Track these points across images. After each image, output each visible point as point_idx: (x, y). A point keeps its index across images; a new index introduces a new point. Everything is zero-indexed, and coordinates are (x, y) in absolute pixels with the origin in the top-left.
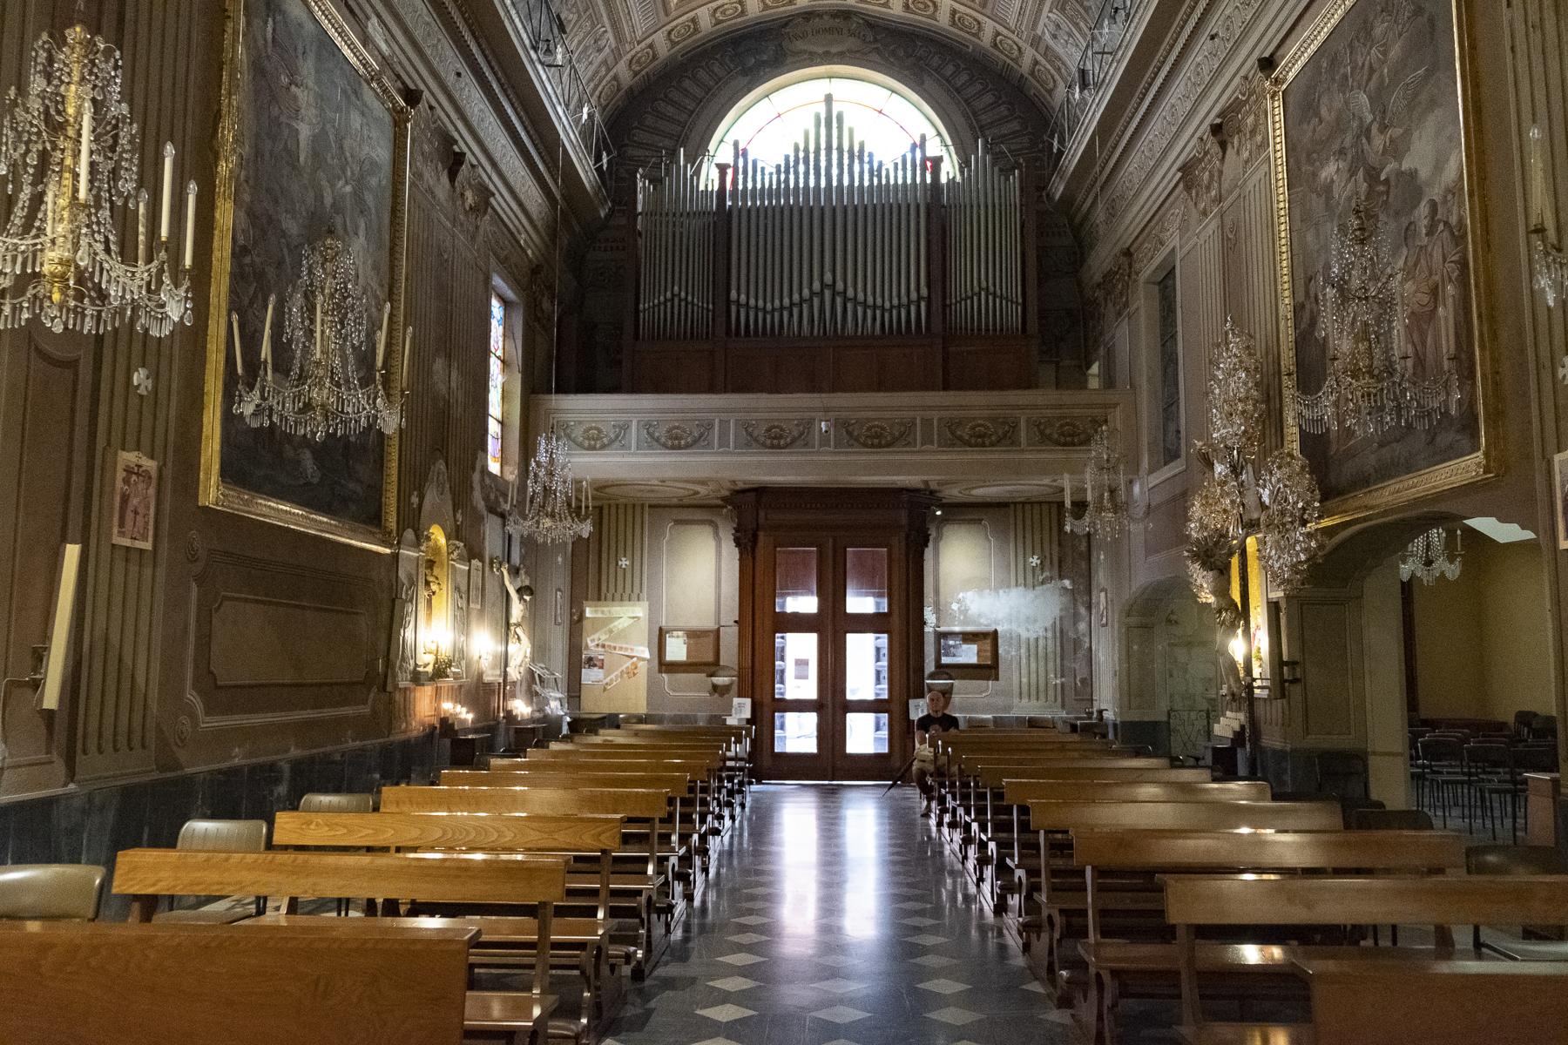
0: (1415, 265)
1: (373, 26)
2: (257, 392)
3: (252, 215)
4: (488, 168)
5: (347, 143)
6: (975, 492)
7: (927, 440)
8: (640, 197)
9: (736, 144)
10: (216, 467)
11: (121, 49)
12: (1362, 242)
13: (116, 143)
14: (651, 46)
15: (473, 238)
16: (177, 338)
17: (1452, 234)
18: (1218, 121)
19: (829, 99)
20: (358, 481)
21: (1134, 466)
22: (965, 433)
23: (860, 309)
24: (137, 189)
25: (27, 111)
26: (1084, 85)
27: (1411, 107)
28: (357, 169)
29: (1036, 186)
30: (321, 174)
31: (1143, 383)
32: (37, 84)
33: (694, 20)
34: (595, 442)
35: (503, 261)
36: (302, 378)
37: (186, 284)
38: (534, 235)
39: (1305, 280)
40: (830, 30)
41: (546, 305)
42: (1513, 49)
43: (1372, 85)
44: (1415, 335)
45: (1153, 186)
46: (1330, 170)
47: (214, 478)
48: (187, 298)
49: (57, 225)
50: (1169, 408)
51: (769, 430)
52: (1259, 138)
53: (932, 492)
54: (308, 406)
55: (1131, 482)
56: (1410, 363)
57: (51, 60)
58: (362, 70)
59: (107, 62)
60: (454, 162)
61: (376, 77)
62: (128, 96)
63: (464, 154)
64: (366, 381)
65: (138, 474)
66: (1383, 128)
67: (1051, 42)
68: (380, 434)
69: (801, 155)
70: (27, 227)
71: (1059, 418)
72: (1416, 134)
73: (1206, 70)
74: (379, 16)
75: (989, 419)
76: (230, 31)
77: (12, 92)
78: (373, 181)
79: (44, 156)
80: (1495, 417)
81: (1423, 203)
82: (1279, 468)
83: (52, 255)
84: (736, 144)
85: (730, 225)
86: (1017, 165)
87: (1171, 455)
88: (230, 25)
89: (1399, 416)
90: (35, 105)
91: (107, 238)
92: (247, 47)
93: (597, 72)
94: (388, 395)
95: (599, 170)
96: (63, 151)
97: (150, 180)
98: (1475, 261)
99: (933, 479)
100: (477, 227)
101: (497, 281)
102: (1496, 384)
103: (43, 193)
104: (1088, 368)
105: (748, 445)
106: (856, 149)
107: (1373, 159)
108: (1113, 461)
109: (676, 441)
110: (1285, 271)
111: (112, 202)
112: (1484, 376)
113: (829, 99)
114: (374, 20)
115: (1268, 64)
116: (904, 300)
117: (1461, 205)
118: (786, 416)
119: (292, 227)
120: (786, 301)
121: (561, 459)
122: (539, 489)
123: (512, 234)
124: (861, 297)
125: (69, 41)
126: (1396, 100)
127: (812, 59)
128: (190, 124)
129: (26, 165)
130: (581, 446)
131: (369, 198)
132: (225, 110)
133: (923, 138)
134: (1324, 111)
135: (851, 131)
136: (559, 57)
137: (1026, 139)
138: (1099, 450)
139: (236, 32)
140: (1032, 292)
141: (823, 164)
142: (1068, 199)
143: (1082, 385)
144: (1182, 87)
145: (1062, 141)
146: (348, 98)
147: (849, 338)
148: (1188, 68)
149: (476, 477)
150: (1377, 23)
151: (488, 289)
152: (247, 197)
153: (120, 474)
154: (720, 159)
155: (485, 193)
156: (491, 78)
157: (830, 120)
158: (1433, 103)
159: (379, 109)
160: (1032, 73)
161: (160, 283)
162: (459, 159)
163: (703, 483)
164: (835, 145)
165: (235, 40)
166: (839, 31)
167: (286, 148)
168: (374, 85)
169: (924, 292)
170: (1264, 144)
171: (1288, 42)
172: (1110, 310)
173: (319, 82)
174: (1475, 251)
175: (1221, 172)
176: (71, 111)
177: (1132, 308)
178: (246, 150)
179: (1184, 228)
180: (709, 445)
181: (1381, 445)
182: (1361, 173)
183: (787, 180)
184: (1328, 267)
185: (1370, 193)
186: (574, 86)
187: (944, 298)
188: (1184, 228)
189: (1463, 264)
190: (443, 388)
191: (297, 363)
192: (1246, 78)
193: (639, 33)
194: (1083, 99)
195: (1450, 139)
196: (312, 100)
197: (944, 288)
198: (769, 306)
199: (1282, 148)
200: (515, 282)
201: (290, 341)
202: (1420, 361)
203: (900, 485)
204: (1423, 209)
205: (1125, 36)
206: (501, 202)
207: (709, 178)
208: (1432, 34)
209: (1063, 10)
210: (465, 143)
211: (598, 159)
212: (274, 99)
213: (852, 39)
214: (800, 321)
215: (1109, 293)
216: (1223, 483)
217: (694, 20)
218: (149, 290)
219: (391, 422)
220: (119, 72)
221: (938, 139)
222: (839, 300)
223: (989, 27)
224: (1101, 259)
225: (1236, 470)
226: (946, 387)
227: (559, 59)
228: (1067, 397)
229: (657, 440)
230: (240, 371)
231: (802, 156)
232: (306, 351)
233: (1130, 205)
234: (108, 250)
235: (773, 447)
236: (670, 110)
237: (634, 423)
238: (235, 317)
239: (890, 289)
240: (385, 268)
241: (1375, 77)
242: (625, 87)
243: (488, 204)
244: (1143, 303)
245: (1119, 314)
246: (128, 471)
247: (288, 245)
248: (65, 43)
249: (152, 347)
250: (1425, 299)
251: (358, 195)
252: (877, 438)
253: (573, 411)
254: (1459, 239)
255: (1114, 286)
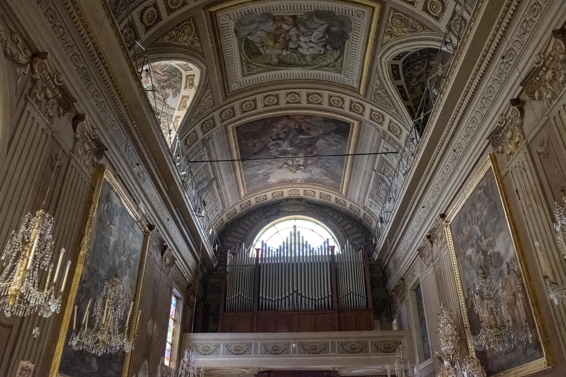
0: (506, 286)
1: (141, 205)
2: (78, 336)
3: (89, 269)
4: (175, 250)
5: (126, 244)
6: (353, 372)
7: (333, 351)
8: (228, 259)
9: (263, 242)
10: (58, 367)
11: (54, 217)
12: (485, 278)
13: (45, 248)
14: (234, 209)
15: (168, 275)
16: (52, 319)
17: (516, 274)
18: (429, 234)
19: (295, 227)
20: (113, 370)
21: (414, 362)
22: (347, 347)
23: (307, 300)
24: (50, 264)
25: (17, 237)
26: (382, 222)
27: (494, 231)
28: (129, 252)
29: (368, 255)
30: (116, 254)
31: (413, 327)
32: (23, 229)
33: (249, 201)
34: (206, 352)
35: (177, 283)
36: (98, 330)
37: (60, 297)
38: (190, 274)
39: (468, 289)
40: (295, 204)
41: (192, 298)
42: (524, 213)
43: (479, 223)
44: (511, 311)
45: (409, 255)
46: (469, 251)
47: (56, 371)
48: (59, 303)
49: (17, 278)
50: (424, 337)
51: (273, 347)
52: (444, 240)
53: (336, 372)
54: (98, 342)
55: (413, 367)
56: (510, 323)
57: (29, 221)
58: (135, 219)
59: (48, 221)
60: (163, 249)
61: (140, 221)
62: (53, 233)
63: (167, 246)
64: (121, 330)
65: (26, 371)
66: (486, 238)
67: (370, 208)
68: (124, 352)
69: (285, 245)
70: (6, 278)
71: (383, 342)
72: (497, 240)
73: (423, 218)
74: (143, 202)
75: (358, 342)
76: (92, 208)
77: (13, 232)
78: (134, 256)
79: (19, 254)
80: (547, 343)
81: (504, 263)
82: (469, 363)
83: (13, 288)
84: (263, 242)
85: (259, 270)
86: (361, 248)
87: (427, 356)
88: (93, 206)
89: (511, 343)
90: (20, 236)
91: (34, 282)
92: (97, 212)
93: (216, 218)
94: (128, 337)
95: (214, 251)
96: (26, 251)
97: (54, 260)
98: (527, 284)
99: (336, 367)
100: (169, 271)
101: (175, 290)
102: (544, 330)
103: (15, 266)
104: (392, 321)
105: (265, 353)
106: (305, 243)
107: (484, 248)
108: (405, 360)
109: (238, 352)
110: (460, 287)
111: (39, 268)
112: (539, 327)
113: (295, 227)
114: (142, 203)
115: (443, 216)
116: (323, 297)
117: (517, 264)
118: (280, 341)
119: (103, 273)
120: (280, 297)
121: (193, 359)
122: (184, 372)
123: (182, 273)
124: (307, 296)
125: (37, 215)
126: (488, 228)
127: (289, 213)
128: (73, 239)
129: (12, 256)
130: (201, 354)
131: (132, 262)
132: (86, 233)
133: (328, 240)
134: (464, 231)
135: (303, 237)
136: (203, 213)
137: (364, 239)
138: (398, 355)
139: (94, 208)
140: (369, 293)
141: (293, 249)
142: (380, 260)
143: (391, 328)
144: (415, 223)
145: (376, 240)
146: (129, 228)
147: (303, 311)
148: (410, 230)
149: (159, 367)
150: (477, 204)
151: (171, 292)
152: (88, 263)
153: (19, 371)
154: (257, 247)
155: (173, 259)
156: (179, 220)
157: (295, 234)
158: (501, 230)
159: (140, 232)
160: (364, 218)
161: (50, 298)
162: (165, 247)
163: (247, 368)
164: (297, 242)
165: (94, 211)
166: (298, 205)
167: (105, 246)
168: (139, 224)
169: (330, 294)
170: (446, 242)
171: (449, 209)
172: (398, 300)
173: (120, 223)
174: (526, 281)
175: (432, 252)
176: (32, 237)
177: (406, 299)
178: (91, 247)
179: (421, 271)
180: (250, 353)
181: (506, 354)
182: (480, 252)
183: (280, 254)
184: (474, 287)
185: (485, 260)
186: (207, 222)
187: (337, 296)
188: (421, 271)
189: (522, 285)
190: (150, 331)
191: (96, 324)
192: (436, 220)
193: (231, 206)
194: (382, 226)
195: (509, 241)
196: (116, 229)
197: (337, 293)
198: (274, 299)
199: (452, 243)
200: (181, 290)
201: (95, 316)
202: (514, 321)
203: (324, 369)
204: (504, 266)
205: (394, 206)
206: (179, 262)
207: (253, 253)
208: (496, 207)
209: (373, 198)
210: (168, 242)
211: (214, 246)
212: (104, 229)
213: (302, 207)
214: (285, 304)
215: (397, 293)
216: (448, 369)
217: (249, 201)
218: (45, 300)
219: (128, 348)
220: (52, 225)
221: (333, 240)
222: (299, 297)
223: (348, 203)
224: (393, 282)
225: (452, 364)
226: (340, 330)
227: (203, 214)
228: (385, 333)
229: (230, 351)
230: (74, 328)
231: (286, 246)
232: (101, 320)
233: (402, 262)
234: (34, 286)
235: (274, 354)
236: (240, 230)
237: (222, 345)
238: (76, 307)
239: (318, 292)
240: (134, 287)
241: (480, 221)
242: (225, 222)
243: (174, 263)
244: (410, 297)
245: (402, 301)
246: (23, 369)
247: (100, 279)
248: (35, 216)
249: (42, 321)
250: (512, 298)
251: (128, 261)
252: (314, 350)
253: (199, 339)
254: (519, 276)
255: (399, 291)
